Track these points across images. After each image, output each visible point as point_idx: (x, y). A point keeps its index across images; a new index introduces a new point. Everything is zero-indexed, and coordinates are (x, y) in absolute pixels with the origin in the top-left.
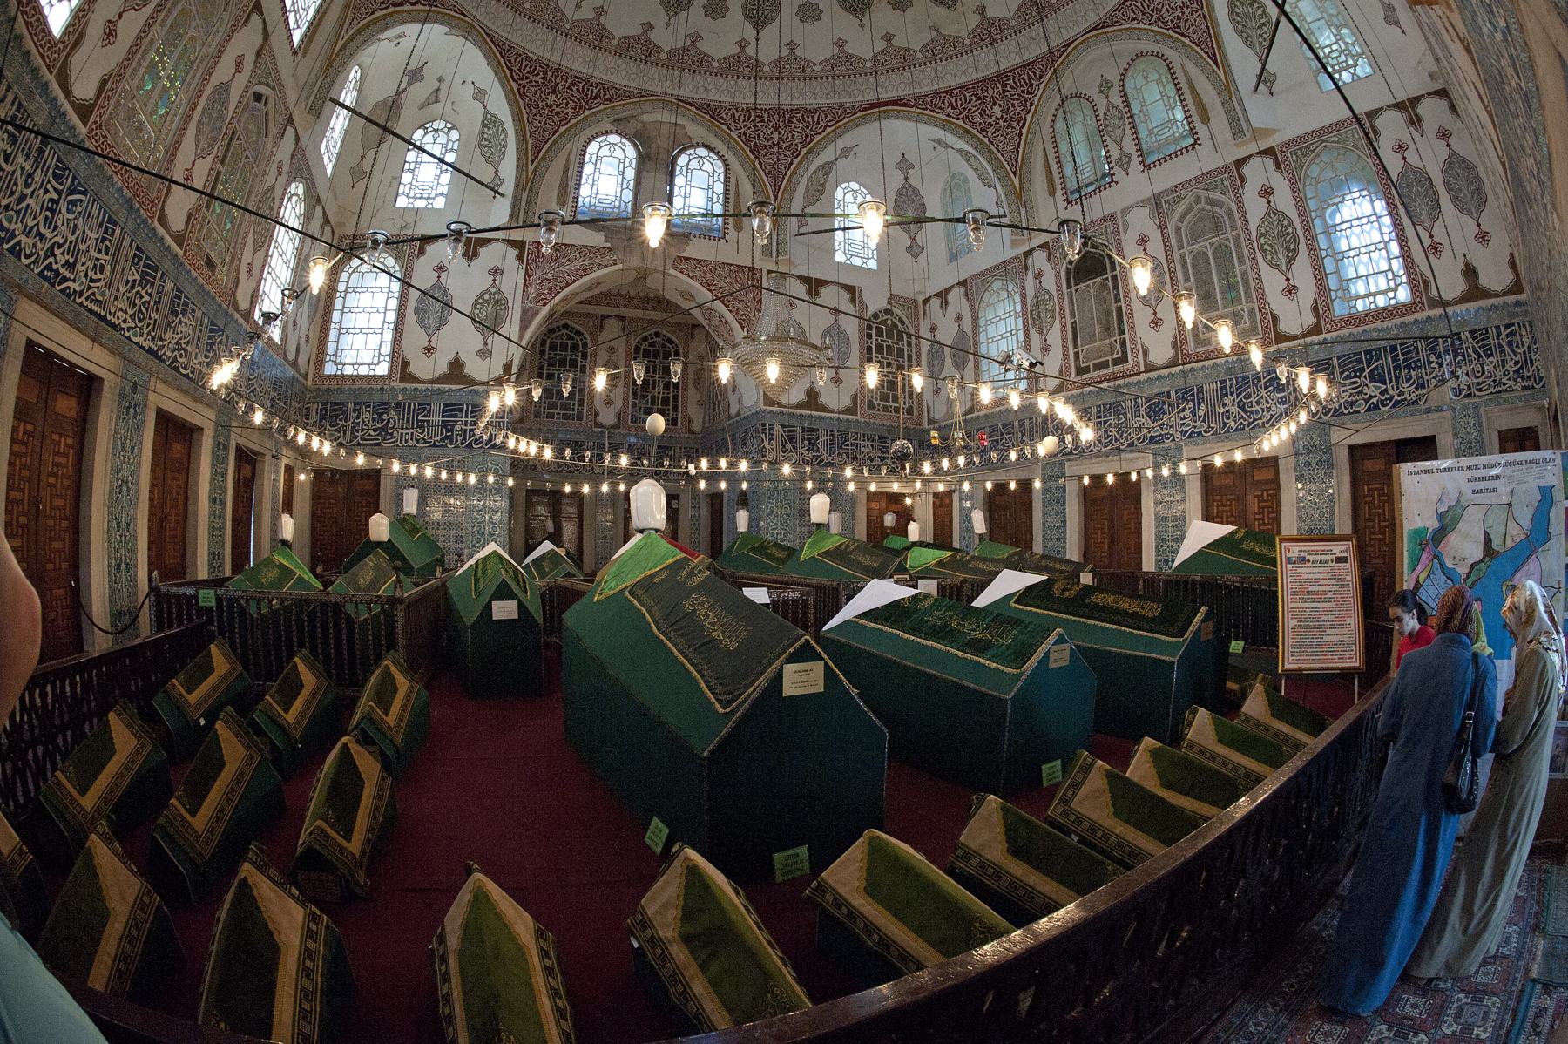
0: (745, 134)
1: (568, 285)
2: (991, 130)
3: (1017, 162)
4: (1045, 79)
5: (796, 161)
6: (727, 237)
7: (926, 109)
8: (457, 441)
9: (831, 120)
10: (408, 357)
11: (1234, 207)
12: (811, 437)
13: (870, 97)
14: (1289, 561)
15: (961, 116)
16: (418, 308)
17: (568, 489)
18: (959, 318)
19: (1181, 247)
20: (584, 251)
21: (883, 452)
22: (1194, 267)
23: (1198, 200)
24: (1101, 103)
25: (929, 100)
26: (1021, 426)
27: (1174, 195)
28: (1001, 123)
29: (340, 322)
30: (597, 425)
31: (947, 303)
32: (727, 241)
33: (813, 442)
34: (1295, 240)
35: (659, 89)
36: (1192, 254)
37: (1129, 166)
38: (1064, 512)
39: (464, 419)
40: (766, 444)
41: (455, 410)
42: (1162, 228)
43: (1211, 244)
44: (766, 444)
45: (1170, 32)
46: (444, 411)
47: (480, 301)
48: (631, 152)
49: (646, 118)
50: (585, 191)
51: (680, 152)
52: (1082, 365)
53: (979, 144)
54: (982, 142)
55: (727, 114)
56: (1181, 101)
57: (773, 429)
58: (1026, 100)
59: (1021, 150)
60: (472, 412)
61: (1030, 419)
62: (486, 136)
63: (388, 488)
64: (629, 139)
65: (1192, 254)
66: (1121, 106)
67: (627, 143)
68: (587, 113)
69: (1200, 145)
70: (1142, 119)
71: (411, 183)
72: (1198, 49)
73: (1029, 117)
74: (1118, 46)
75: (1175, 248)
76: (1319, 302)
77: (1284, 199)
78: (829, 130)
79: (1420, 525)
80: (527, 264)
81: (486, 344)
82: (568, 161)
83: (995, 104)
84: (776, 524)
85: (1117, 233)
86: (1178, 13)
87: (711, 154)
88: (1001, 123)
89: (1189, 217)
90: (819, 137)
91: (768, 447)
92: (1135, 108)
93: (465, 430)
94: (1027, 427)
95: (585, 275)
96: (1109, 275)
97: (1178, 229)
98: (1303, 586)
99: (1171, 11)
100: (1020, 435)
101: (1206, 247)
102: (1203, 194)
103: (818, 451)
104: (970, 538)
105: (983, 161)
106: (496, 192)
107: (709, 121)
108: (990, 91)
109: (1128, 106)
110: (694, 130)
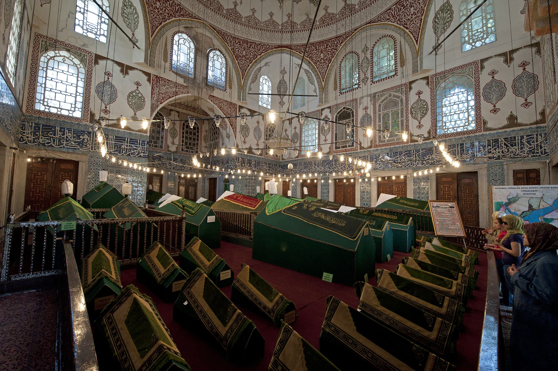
1: (170, 97)
2: (318, 63)
4: (343, 44)
5: (250, 65)
7: (297, 51)
8: (122, 152)
11: (404, 98)
12: (250, 162)
13: (279, 43)
14: (433, 207)
17: (183, 176)
18: (295, 128)
19: (379, 111)
20: (176, 85)
22: (383, 118)
23: (390, 95)
24: (362, 56)
27: (382, 93)
29: (68, 110)
30: (169, 151)
31: (291, 123)
34: (426, 110)
35: (202, 17)
38: (328, 189)
40: (237, 163)
41: (121, 140)
42: (374, 105)
44: (237, 163)
45: (402, 27)
47: (131, 95)
48: (192, 46)
50: (175, 58)
53: (313, 68)
54: (314, 68)
56: (395, 57)
58: (333, 52)
60: (130, 142)
62: (125, 11)
63: (84, 169)
64: (191, 38)
66: (370, 58)
68: (174, 19)
69: (397, 75)
70: (377, 64)
72: (411, 35)
73: (333, 59)
74: (374, 31)
75: (377, 111)
76: (431, 130)
77: (426, 96)
79: (500, 201)
80: (152, 84)
81: (135, 114)
82: (166, 41)
83: (322, 53)
85: (356, 105)
86: (409, 17)
87: (221, 55)
89: (385, 101)
90: (260, 56)
92: (375, 59)
96: (351, 119)
97: (380, 105)
98: (439, 214)
99: (406, 16)
101: (389, 112)
102: (392, 93)
105: (313, 75)
106: (134, 44)
109: (372, 58)
110: (217, 43)
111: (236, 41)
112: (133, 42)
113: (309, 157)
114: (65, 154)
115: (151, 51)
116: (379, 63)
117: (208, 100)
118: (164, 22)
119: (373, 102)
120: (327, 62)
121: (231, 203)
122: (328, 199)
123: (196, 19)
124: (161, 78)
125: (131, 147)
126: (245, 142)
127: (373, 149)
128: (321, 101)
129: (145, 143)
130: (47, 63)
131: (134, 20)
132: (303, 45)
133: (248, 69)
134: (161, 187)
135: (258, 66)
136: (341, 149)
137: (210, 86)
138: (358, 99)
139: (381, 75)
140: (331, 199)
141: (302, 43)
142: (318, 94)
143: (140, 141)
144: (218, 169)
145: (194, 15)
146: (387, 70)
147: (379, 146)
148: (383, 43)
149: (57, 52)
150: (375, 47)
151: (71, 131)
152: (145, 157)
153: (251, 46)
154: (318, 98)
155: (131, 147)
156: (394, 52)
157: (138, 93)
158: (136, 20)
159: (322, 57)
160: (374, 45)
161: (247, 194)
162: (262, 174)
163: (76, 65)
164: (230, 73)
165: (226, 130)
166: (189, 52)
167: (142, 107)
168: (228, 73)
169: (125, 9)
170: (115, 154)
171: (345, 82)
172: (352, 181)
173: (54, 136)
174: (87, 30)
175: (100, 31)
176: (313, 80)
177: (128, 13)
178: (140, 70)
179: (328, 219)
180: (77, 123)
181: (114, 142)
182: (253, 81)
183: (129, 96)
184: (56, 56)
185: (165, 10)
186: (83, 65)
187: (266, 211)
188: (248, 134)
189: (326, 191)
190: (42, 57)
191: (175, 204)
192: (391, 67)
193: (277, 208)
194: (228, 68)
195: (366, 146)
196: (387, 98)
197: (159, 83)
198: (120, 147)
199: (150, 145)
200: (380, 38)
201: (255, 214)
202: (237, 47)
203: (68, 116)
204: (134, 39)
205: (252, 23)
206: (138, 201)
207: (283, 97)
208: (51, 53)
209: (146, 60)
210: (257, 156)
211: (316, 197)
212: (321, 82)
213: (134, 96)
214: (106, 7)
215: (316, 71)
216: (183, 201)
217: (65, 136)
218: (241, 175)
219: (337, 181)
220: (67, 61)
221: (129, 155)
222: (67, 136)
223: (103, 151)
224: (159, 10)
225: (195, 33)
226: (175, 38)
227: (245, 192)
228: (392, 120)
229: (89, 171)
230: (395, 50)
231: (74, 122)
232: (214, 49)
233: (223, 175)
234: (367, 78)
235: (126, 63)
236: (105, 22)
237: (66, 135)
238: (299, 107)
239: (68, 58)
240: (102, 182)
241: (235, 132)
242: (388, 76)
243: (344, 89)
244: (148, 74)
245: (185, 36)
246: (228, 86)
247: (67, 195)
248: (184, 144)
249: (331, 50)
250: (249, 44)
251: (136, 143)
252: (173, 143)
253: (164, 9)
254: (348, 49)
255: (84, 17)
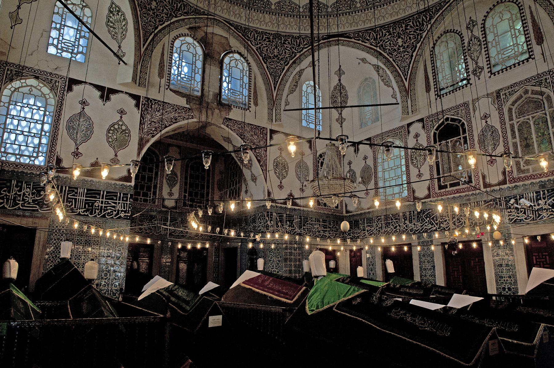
0: (260, 48)
1: (166, 127)
2: (395, 54)
3: (408, 73)
6: (250, 109)
7: (359, 40)
8: (95, 212)
9: (306, 44)
10: (62, 156)
15: (378, 45)
16: (69, 126)
18: (365, 158)
19: (511, 119)
20: (176, 108)
21: (324, 228)
22: (519, 130)
23: (526, 92)
25: (361, 35)
26: (404, 215)
27: (510, 90)
28: (401, 49)
30: (164, 206)
31: (358, 150)
32: (250, 111)
33: (291, 221)
36: (518, 124)
37: (480, 74)
39: (101, 200)
40: (269, 222)
41: (94, 193)
43: (533, 117)
44: (269, 222)
46: (87, 194)
47: (112, 128)
49: (210, 30)
51: (225, 55)
52: (442, 184)
53: (387, 62)
55: (250, 34)
56: (524, 31)
57: (272, 215)
58: (418, 35)
59: (411, 65)
60: (106, 196)
61: (409, 212)
62: (111, 19)
64: (198, 42)
65: (518, 124)
67: (197, 44)
68: (174, 19)
70: (494, 45)
71: (58, 39)
76: (431, 185)
78: (305, 50)
80: (142, 110)
81: (116, 155)
82: (163, 49)
83: (399, 37)
84: (273, 266)
85: (468, 113)
87: (242, 59)
88: (401, 49)
91: (270, 224)
92: (490, 38)
93: (102, 207)
94: (408, 216)
95: (176, 122)
96: (462, 136)
97: (510, 110)
100: (403, 220)
101: (529, 119)
102: (530, 88)
103: (293, 227)
104: (373, 274)
105: (388, 72)
106: (120, 59)
107: (241, 37)
108: (398, 29)
109: (485, 37)
110: (234, 43)
111: (263, 37)
112: (118, 56)
113: (190, 244)
114: (20, 218)
115: (142, 66)
116: (498, 43)
117: (222, 126)
118: (161, 25)
119: (496, 106)
120: (409, 50)
121: (254, 291)
122: (435, 280)
123: (206, 15)
124: (155, 100)
125: (108, 203)
126: (281, 187)
127: (508, 185)
128: (405, 111)
129: (127, 198)
130: (10, 97)
131: (122, 28)
132: (367, 30)
133: (283, 74)
134: (150, 265)
135: (298, 69)
136: (449, 189)
137: (225, 104)
138: (471, 102)
139: (504, 61)
140: (440, 281)
141: (365, 27)
142: (399, 101)
143: (120, 194)
144: (233, 233)
145: (202, 11)
146: (513, 52)
147: (520, 179)
148: (500, 12)
149: (23, 81)
150: (488, 19)
151: (30, 185)
152: (127, 219)
153: (285, 41)
154: (400, 106)
155: (108, 203)
156: (521, 23)
157: (122, 125)
158: (124, 28)
159: (400, 44)
160: (485, 16)
161: (288, 275)
162: (308, 239)
163: (44, 95)
164: (255, 84)
165: (250, 170)
166: (194, 61)
167: (126, 145)
168: (253, 83)
169: (110, 17)
170: (85, 215)
171: (445, 78)
172: (475, 245)
173: (8, 194)
174: (62, 49)
175: (78, 48)
176: (389, 79)
177: (115, 20)
178: (126, 93)
179: (418, 322)
180: (38, 173)
181: (84, 198)
182: (292, 91)
183: (109, 131)
184: (22, 87)
185: (163, 10)
186: (53, 95)
187: (307, 307)
188: (287, 174)
189: (428, 266)
190: (6, 90)
191: (161, 293)
192: (520, 46)
193: (326, 301)
194: (253, 76)
195: (494, 181)
196: (521, 97)
197: (151, 107)
198: (93, 204)
199: (136, 200)
200: (494, 6)
201: (291, 311)
202: (264, 45)
203: (28, 165)
204: (120, 54)
205: (287, 10)
206: (114, 288)
207: (341, 111)
208: (16, 84)
209: (134, 79)
210: (280, 205)
211: (411, 276)
212: (402, 81)
213: (116, 129)
214: (88, 17)
215: (393, 66)
216: (173, 289)
217: (22, 193)
218: (274, 241)
219: (446, 246)
220: (35, 91)
221: (104, 216)
222: (24, 193)
223: (60, 214)
224: (155, 11)
225: (203, 34)
226: (175, 45)
227: (283, 272)
228: (537, 132)
229: (48, 241)
230: (522, 21)
231: (35, 172)
232: (232, 52)
233: (244, 242)
234: (482, 68)
235: (108, 85)
236: (84, 36)
237: (23, 192)
238: (369, 123)
239: (35, 87)
240: (63, 259)
241: (265, 170)
242: (517, 61)
243: (443, 89)
244: (136, 97)
245: (189, 40)
246: (252, 103)
247: (11, 280)
248: (187, 195)
249: (414, 32)
250: (283, 39)
251: (115, 198)
252: (171, 194)
253: (161, 8)
254: (441, 28)
255: (60, 33)
